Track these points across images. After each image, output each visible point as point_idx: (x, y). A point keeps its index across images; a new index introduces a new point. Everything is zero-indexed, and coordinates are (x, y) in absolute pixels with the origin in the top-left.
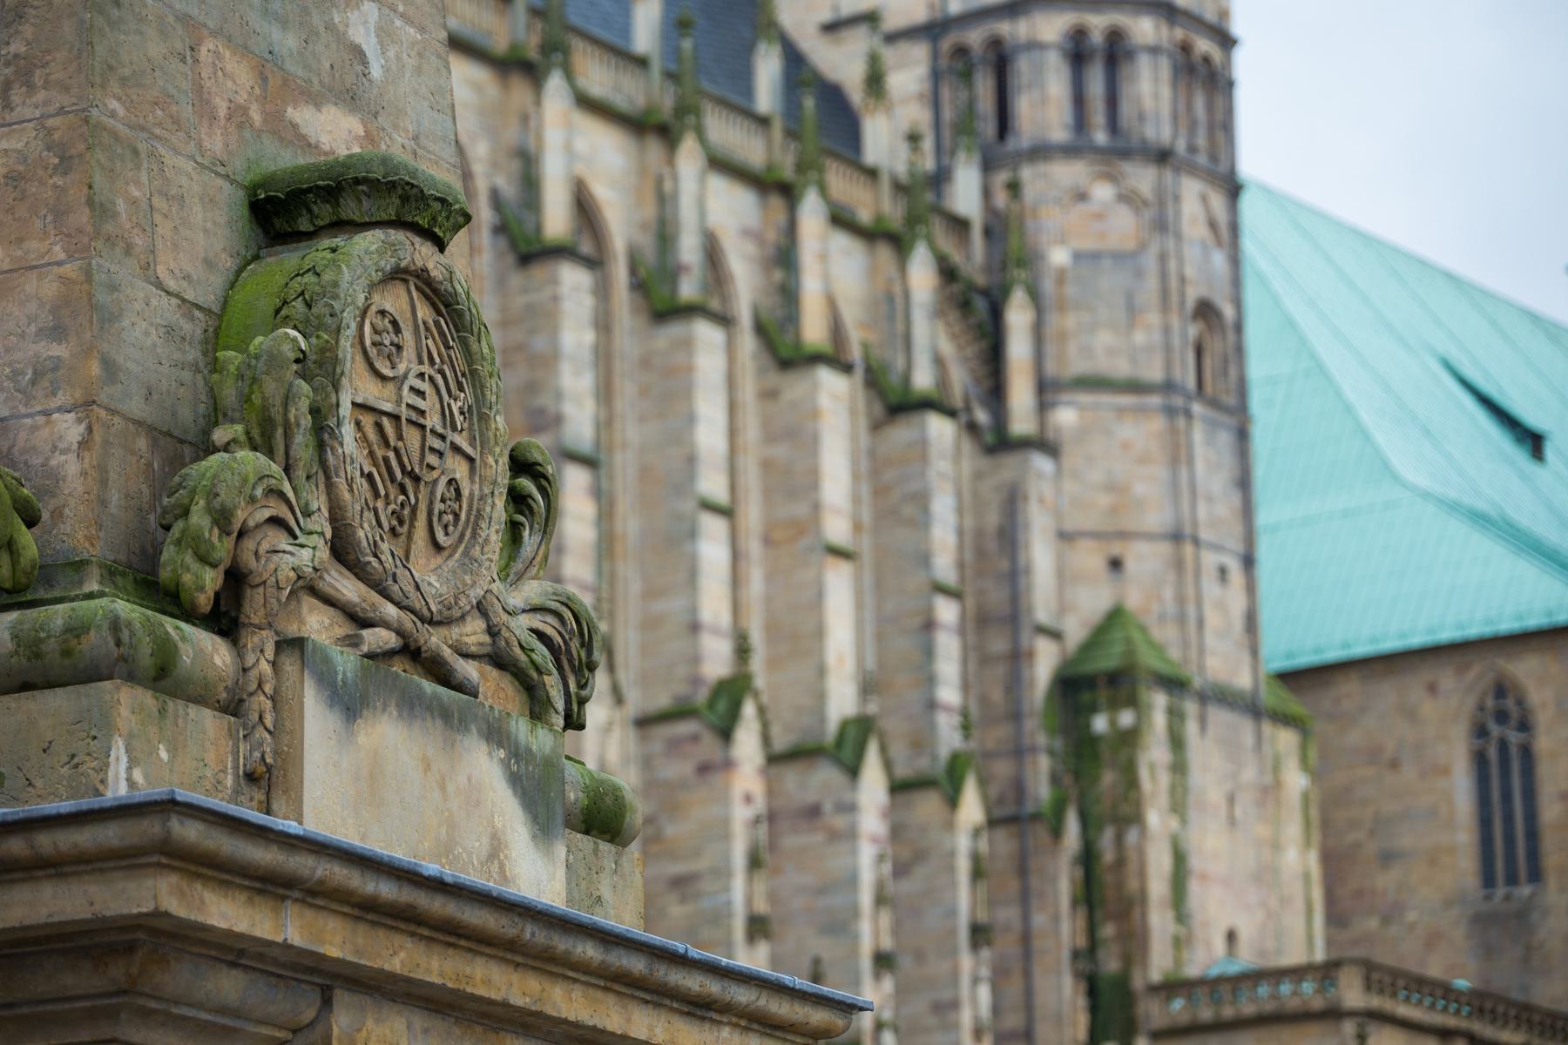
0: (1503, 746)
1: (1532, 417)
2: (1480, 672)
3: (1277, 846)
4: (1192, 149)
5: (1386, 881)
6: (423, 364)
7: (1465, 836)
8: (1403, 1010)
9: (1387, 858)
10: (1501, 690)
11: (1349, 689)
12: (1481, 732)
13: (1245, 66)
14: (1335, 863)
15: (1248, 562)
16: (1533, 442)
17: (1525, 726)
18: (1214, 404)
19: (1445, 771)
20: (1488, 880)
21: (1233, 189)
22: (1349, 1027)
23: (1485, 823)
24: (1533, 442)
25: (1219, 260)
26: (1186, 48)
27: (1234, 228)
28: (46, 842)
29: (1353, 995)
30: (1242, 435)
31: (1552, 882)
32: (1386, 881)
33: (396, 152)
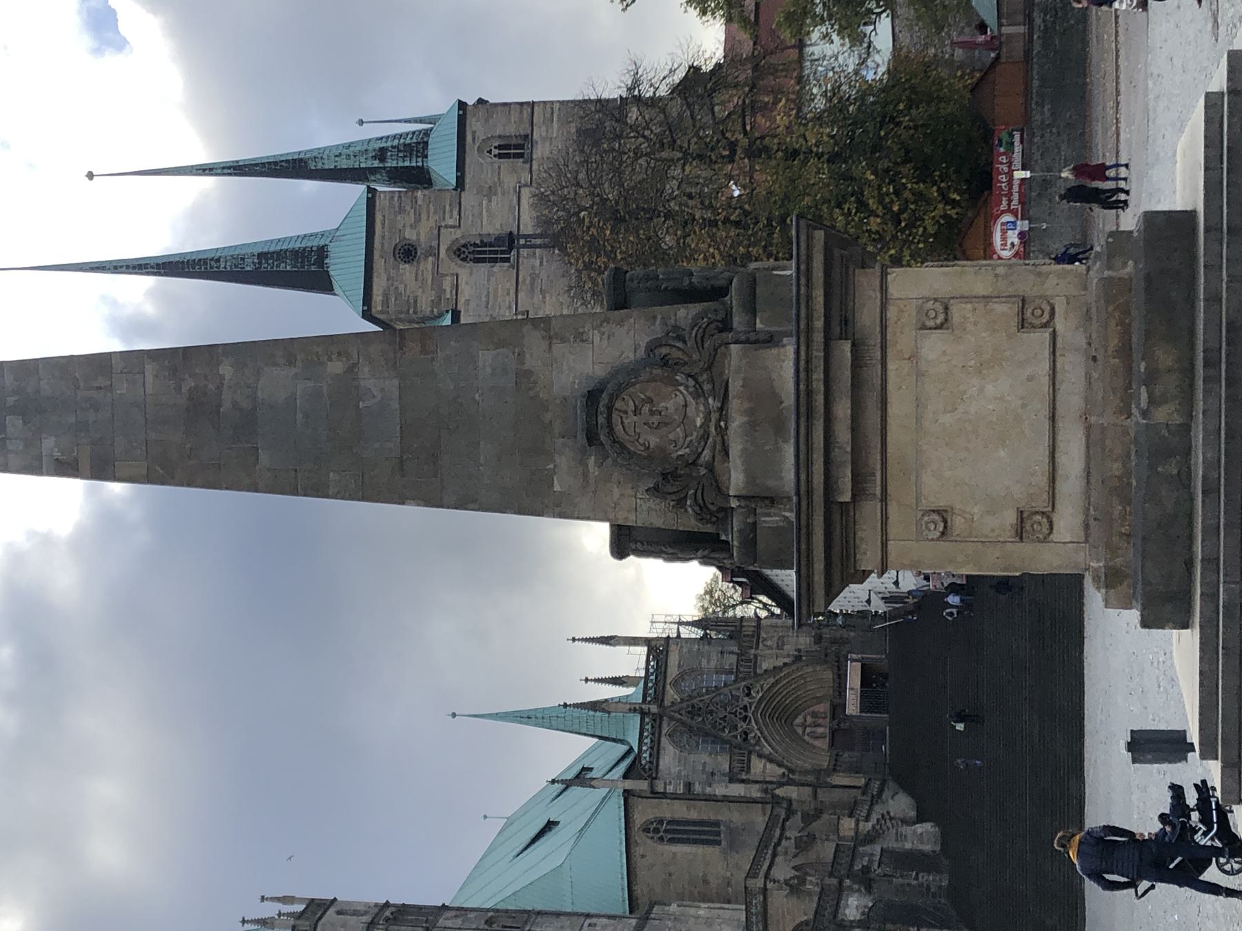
0: (666, 831)
1: (541, 824)
2: (639, 837)
3: (698, 917)
4: (427, 921)
5: (714, 883)
6: (524, 153)
7: (699, 850)
8: (765, 867)
9: (705, 882)
10: (647, 830)
11: (639, 889)
12: (661, 839)
13: (396, 900)
14: (705, 898)
15: (588, 916)
16: (550, 825)
17: (661, 822)
18: (526, 922)
19: (675, 854)
20: (719, 843)
21: (444, 908)
22: (770, 885)
23: (695, 842)
24: (550, 825)
25: (471, 915)
26: (387, 920)
27: (459, 909)
28: (803, 522)
29: (759, 882)
30: (539, 913)
31: (720, 818)
32: (714, 883)
33: (381, 292)
